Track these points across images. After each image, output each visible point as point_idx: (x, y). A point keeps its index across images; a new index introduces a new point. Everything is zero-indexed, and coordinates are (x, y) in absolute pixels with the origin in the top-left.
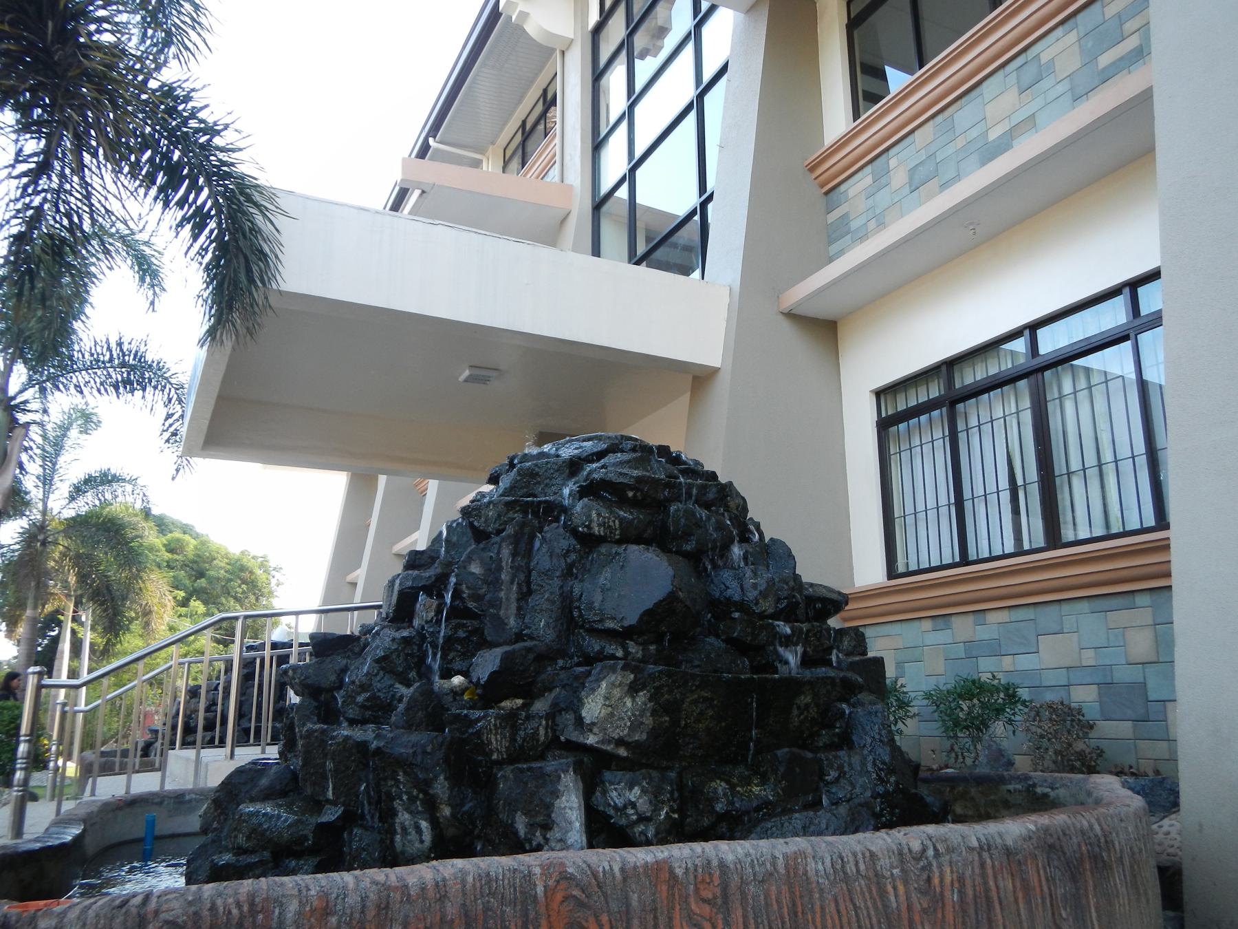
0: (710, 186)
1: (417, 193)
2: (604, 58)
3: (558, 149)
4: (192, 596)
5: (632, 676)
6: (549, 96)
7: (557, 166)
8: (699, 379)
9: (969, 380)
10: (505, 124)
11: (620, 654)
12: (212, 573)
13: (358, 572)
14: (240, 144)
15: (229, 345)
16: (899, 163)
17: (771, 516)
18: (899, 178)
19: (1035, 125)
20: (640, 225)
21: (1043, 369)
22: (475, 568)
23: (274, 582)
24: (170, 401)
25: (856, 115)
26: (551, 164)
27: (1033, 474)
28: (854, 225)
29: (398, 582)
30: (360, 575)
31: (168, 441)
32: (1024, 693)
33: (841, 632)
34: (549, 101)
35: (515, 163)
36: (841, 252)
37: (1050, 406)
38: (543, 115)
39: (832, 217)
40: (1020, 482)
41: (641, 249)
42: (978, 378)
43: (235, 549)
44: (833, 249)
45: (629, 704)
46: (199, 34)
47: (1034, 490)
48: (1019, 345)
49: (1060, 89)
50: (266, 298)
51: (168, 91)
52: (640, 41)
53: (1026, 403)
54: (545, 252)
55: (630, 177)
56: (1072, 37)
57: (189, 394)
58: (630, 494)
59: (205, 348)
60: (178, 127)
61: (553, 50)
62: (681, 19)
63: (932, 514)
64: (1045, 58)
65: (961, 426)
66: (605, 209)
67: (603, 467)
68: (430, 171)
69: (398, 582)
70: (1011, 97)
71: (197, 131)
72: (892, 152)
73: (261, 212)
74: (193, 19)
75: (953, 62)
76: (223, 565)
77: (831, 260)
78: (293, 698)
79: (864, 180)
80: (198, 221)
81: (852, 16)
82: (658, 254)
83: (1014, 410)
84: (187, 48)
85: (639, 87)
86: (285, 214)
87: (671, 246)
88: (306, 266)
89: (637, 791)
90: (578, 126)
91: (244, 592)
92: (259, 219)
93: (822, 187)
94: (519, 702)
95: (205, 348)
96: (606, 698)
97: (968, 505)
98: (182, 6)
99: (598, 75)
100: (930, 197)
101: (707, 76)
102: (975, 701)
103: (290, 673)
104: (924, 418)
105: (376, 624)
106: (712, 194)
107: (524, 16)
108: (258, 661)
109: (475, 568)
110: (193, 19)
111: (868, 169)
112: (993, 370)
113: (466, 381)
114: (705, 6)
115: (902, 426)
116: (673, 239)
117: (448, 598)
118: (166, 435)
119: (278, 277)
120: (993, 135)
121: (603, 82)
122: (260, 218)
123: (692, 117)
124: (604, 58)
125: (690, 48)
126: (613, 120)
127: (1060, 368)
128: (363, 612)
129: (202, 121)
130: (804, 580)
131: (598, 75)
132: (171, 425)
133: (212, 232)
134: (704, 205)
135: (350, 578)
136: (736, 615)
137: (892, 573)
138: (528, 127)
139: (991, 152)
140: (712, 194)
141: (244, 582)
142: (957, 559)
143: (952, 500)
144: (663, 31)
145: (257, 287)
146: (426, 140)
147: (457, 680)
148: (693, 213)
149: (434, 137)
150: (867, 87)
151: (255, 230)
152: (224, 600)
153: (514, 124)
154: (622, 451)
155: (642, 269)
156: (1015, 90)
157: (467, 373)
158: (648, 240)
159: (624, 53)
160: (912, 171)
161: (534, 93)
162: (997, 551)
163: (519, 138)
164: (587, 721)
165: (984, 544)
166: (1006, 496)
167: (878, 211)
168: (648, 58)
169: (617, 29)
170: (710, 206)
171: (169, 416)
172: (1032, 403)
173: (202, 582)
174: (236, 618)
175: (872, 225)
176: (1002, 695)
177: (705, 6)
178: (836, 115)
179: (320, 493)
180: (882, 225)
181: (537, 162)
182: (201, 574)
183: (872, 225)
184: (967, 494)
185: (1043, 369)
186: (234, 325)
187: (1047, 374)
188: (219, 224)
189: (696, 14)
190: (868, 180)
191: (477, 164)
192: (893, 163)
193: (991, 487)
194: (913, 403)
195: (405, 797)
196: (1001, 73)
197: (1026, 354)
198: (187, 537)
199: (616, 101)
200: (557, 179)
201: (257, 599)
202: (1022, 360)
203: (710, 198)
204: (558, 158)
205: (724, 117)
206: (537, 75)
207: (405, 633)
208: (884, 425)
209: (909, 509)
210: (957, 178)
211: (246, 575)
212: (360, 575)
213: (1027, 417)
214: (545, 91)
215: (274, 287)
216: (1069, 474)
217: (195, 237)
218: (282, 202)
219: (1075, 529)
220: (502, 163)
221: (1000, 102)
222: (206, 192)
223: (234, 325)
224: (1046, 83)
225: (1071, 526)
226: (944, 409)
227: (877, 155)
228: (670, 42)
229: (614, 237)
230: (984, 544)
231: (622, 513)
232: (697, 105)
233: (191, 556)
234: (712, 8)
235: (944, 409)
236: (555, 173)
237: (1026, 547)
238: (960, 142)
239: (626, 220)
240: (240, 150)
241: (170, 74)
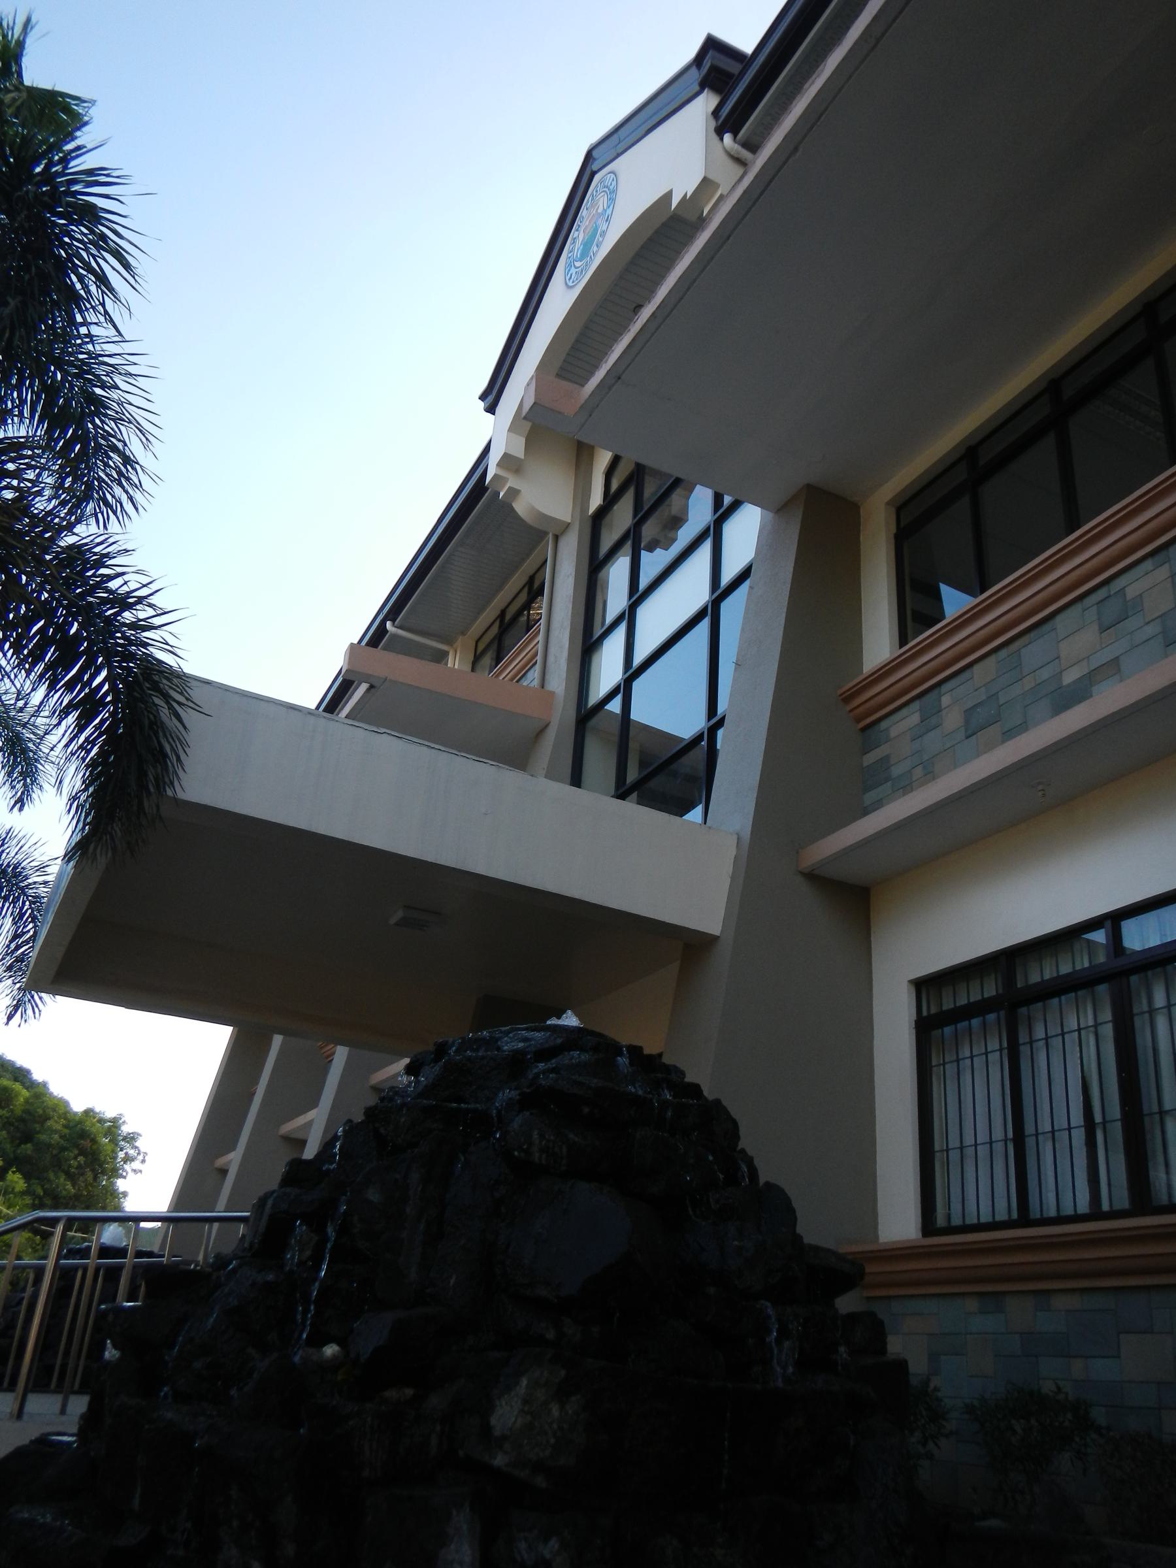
0: (722, 708)
1: (364, 687)
2: (605, 546)
3: (540, 647)
4: (11, 1166)
5: (563, 1373)
6: (536, 584)
7: (538, 667)
8: (692, 947)
9: (1035, 978)
10: (479, 613)
11: (551, 1335)
12: (43, 1137)
13: (232, 1155)
14: (157, 621)
15: (102, 861)
16: (953, 703)
17: (773, 1149)
18: (952, 719)
19: (1119, 670)
20: (633, 746)
21: (1127, 972)
22: (373, 1195)
23: (121, 1155)
24: (21, 918)
25: (903, 641)
26: (530, 664)
27: (1115, 1111)
28: (896, 771)
29: (270, 1202)
30: (233, 1159)
31: (9, 968)
32: (1099, 1415)
33: (853, 1318)
34: (534, 590)
35: (487, 660)
36: (878, 805)
37: (1138, 1022)
38: (527, 606)
39: (870, 759)
40: (1098, 1118)
41: (632, 775)
42: (1047, 976)
43: (78, 1106)
44: (870, 797)
45: (555, 1412)
46: (127, 492)
47: (1117, 1130)
48: (1099, 936)
49: (1150, 630)
50: (158, 806)
51: (78, 552)
52: (649, 530)
53: (1107, 1015)
54: (511, 777)
55: (625, 689)
56: (1163, 573)
57: (47, 910)
58: (586, 1110)
59: (72, 864)
60: (82, 596)
61: (546, 533)
62: (699, 507)
63: (983, 1151)
64: (1131, 593)
65: (1023, 1037)
66: (593, 723)
67: (552, 1070)
68: (385, 663)
69: (270, 1202)
70: (1087, 638)
71: (104, 601)
72: (945, 687)
73: (168, 703)
74: (120, 473)
75: (1024, 587)
76: (59, 1127)
77: (866, 812)
78: (110, 1353)
79: (910, 719)
80: (87, 708)
81: (902, 525)
82: (653, 784)
83: (1091, 1022)
84: (107, 504)
85: (643, 583)
86: (197, 709)
87: (668, 776)
88: (209, 777)
89: (554, 1544)
90: (567, 624)
91: (79, 1167)
92: (164, 714)
93: (858, 720)
94: (409, 1392)
95: (72, 864)
96: (525, 1402)
97: (1030, 1142)
98: (110, 458)
99: (594, 568)
100: (990, 747)
101: (727, 576)
102: (1033, 1422)
103: (111, 1318)
104: (975, 1022)
105: (235, 1257)
106: (723, 718)
107: (514, 493)
108: (80, 1274)
109: (373, 1195)
110: (120, 473)
111: (916, 705)
112: (1065, 969)
113: (397, 924)
114: (727, 500)
115: (948, 1030)
116: (674, 766)
117: (330, 1231)
118: (9, 961)
119: (176, 783)
120: (1069, 678)
121: (602, 575)
122: (166, 711)
123: (704, 625)
124: (605, 546)
125: (705, 550)
126: (609, 619)
127: (1150, 973)
128: (226, 1225)
129: (110, 592)
130: (806, 1241)
131: (594, 568)
132: (18, 947)
133: (103, 721)
134: (712, 731)
135: (220, 1162)
136: (712, 1290)
137: (928, 1226)
138: (508, 617)
139: (1066, 699)
140: (723, 718)
141: (82, 1152)
142: (1015, 1215)
143: (1010, 1135)
144: (677, 521)
145: (149, 793)
146: (383, 623)
147: (330, 1350)
148: (698, 739)
149: (393, 621)
150: (916, 612)
151: (157, 726)
152: (51, 1175)
153: (489, 614)
154: (582, 1049)
155: (630, 808)
156: (1095, 627)
157: (400, 914)
158: (642, 764)
159: (629, 543)
160: (969, 713)
161: (517, 581)
162: (1068, 1210)
163: (495, 630)
164: (497, 1432)
165: (1050, 1197)
166: (1079, 1136)
167: (926, 757)
168: (658, 550)
169: (622, 517)
170: (720, 733)
171: (16, 936)
172: (1114, 1014)
173: (28, 1148)
174: (54, 1222)
175: (919, 772)
176: (1069, 1416)
177: (727, 500)
178: (879, 642)
179: (194, 1050)
180: (930, 775)
181: (513, 662)
182: (27, 1137)
183: (919, 772)
184: (1029, 1129)
185: (1127, 972)
186: (112, 838)
187: (1134, 979)
188: (113, 714)
189: (716, 509)
190: (915, 718)
191: (440, 657)
192: (946, 700)
193: (1061, 1122)
194: (962, 1001)
195: (235, 1523)
196: (1078, 607)
197: (1106, 946)
198: (17, 1086)
199: (616, 599)
200: (536, 683)
201: (95, 1178)
202: (1101, 958)
203: (721, 723)
204: (539, 658)
205: (743, 630)
206: (523, 560)
207: (271, 1277)
208: (926, 1029)
209: (954, 1142)
210: (1023, 727)
211: (86, 1143)
212: (233, 1159)
213: (1108, 1031)
214: (532, 579)
215: (169, 793)
216: (1162, 1113)
217: (81, 728)
218: (196, 694)
219: (1168, 1173)
220: (471, 657)
221: (1076, 642)
222: (104, 674)
223: (112, 838)
224: (1131, 623)
225: (1162, 1168)
226: (1002, 1013)
227: (924, 691)
228: (685, 535)
229: (600, 761)
230: (1050, 1197)
231: (571, 1136)
232: (711, 612)
233: (18, 1112)
234: (735, 506)
235: (1002, 1013)
236: (534, 675)
237: (1105, 1207)
238: (1028, 683)
239: (616, 739)
240: (156, 628)
241: (85, 531)
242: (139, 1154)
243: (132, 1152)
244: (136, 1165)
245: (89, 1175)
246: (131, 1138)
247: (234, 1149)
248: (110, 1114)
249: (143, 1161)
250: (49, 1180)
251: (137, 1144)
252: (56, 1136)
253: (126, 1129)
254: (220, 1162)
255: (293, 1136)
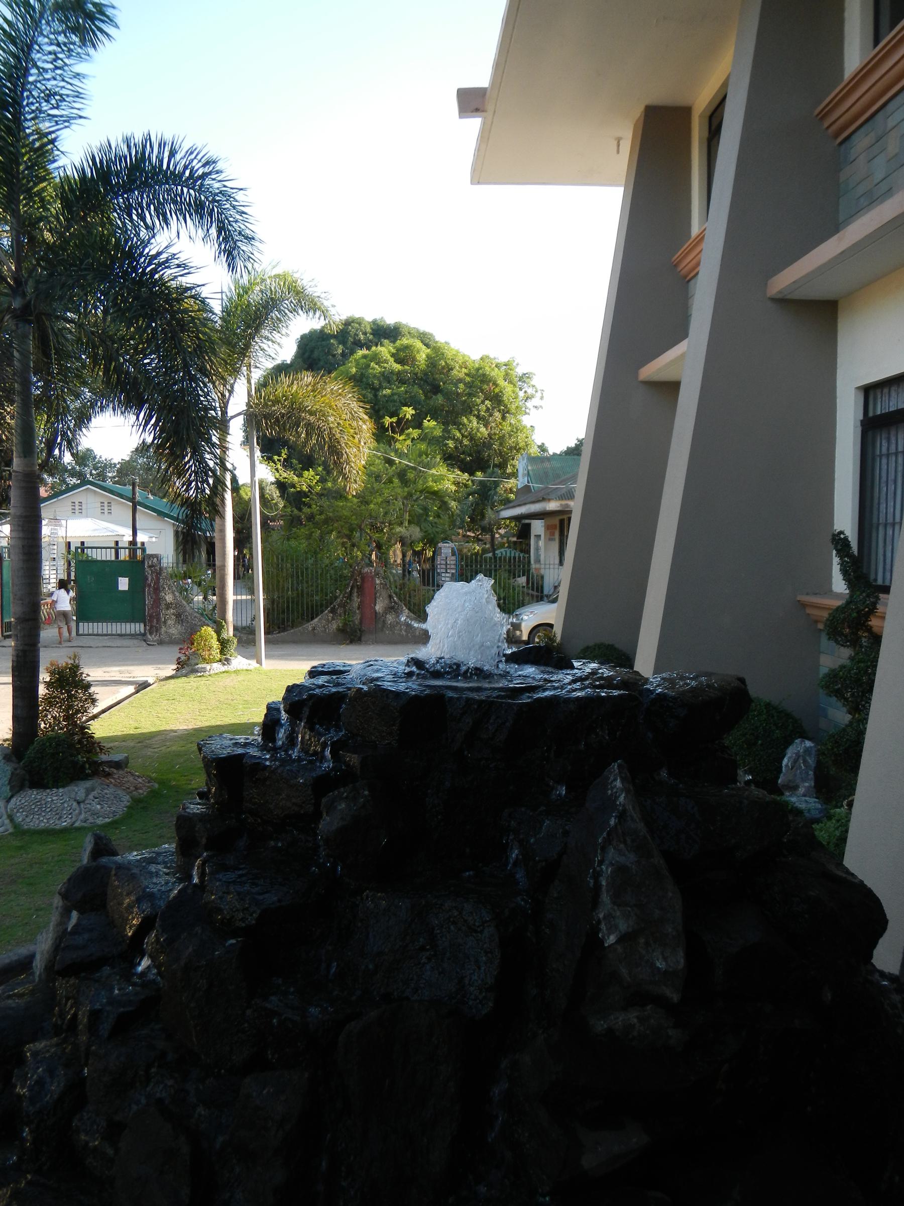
28: (521, 445)
30: (684, 360)
76: (462, 375)
135: (657, 368)
173: (440, 399)
212: (684, 360)
242: (536, 391)
243: (530, 391)
244: (535, 401)
245: (497, 415)
246: (525, 378)
247: (685, 335)
248: (503, 359)
249: (542, 398)
250: (464, 425)
251: (532, 383)
252: (461, 386)
253: (520, 371)
254: (657, 368)
255: (797, 295)
